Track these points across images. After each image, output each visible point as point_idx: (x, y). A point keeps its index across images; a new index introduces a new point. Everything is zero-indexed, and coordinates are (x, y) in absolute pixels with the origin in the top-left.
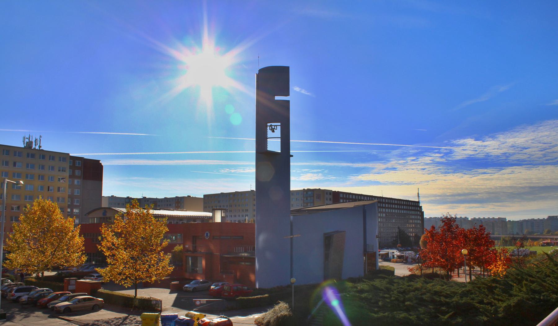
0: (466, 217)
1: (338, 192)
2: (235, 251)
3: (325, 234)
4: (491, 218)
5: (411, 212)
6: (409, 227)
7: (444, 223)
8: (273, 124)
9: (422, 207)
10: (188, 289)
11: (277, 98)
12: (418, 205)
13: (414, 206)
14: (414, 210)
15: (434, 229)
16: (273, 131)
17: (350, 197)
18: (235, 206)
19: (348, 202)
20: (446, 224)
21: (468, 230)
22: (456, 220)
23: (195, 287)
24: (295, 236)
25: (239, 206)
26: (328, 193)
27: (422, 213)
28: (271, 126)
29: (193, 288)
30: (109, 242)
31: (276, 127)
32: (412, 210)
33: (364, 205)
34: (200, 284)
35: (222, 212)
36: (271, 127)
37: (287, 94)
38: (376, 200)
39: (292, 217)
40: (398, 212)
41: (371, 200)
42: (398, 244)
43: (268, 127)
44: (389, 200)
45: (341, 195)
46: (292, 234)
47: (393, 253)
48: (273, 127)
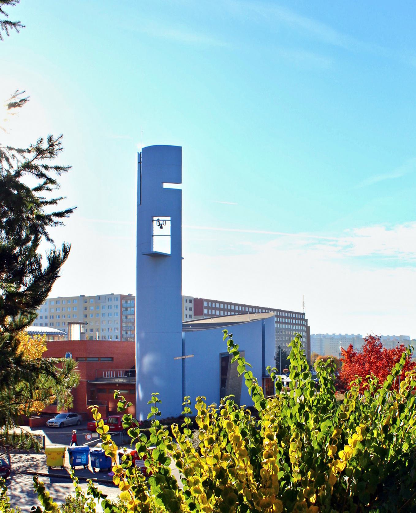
0: (359, 334)
1: (201, 299)
2: (104, 377)
3: (221, 354)
4: (391, 336)
5: (294, 326)
6: (97, 340)
7: (367, 342)
8: (160, 218)
9: (308, 321)
10: (54, 424)
11: (166, 186)
12: (304, 318)
13: (298, 319)
14: (298, 324)
15: (352, 348)
16: (161, 227)
17: (217, 307)
18: (58, 317)
19: (238, 315)
20: (370, 343)
21: (390, 350)
22: (380, 338)
23: (62, 421)
24: (180, 358)
25: (65, 317)
26: (188, 301)
27: (308, 328)
28: (158, 220)
29: (60, 423)
30: (388, 356)
31: (164, 222)
32: (296, 324)
33: (263, 319)
34: (68, 418)
35: (82, 327)
36: (158, 222)
37: (179, 181)
38: (272, 314)
39: (183, 334)
40: (278, 327)
41: (267, 313)
42: (285, 368)
43: (155, 223)
44: (240, 307)
45: (205, 304)
46: (183, 354)
47: (283, 379)
48: (161, 222)
